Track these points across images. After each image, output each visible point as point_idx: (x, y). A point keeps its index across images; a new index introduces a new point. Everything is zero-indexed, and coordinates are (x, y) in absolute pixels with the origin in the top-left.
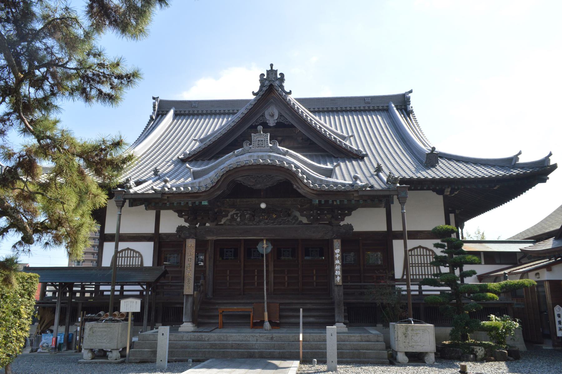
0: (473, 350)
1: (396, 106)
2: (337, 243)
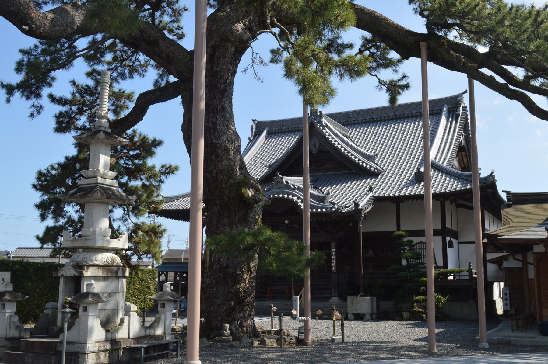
2: (333, 245)
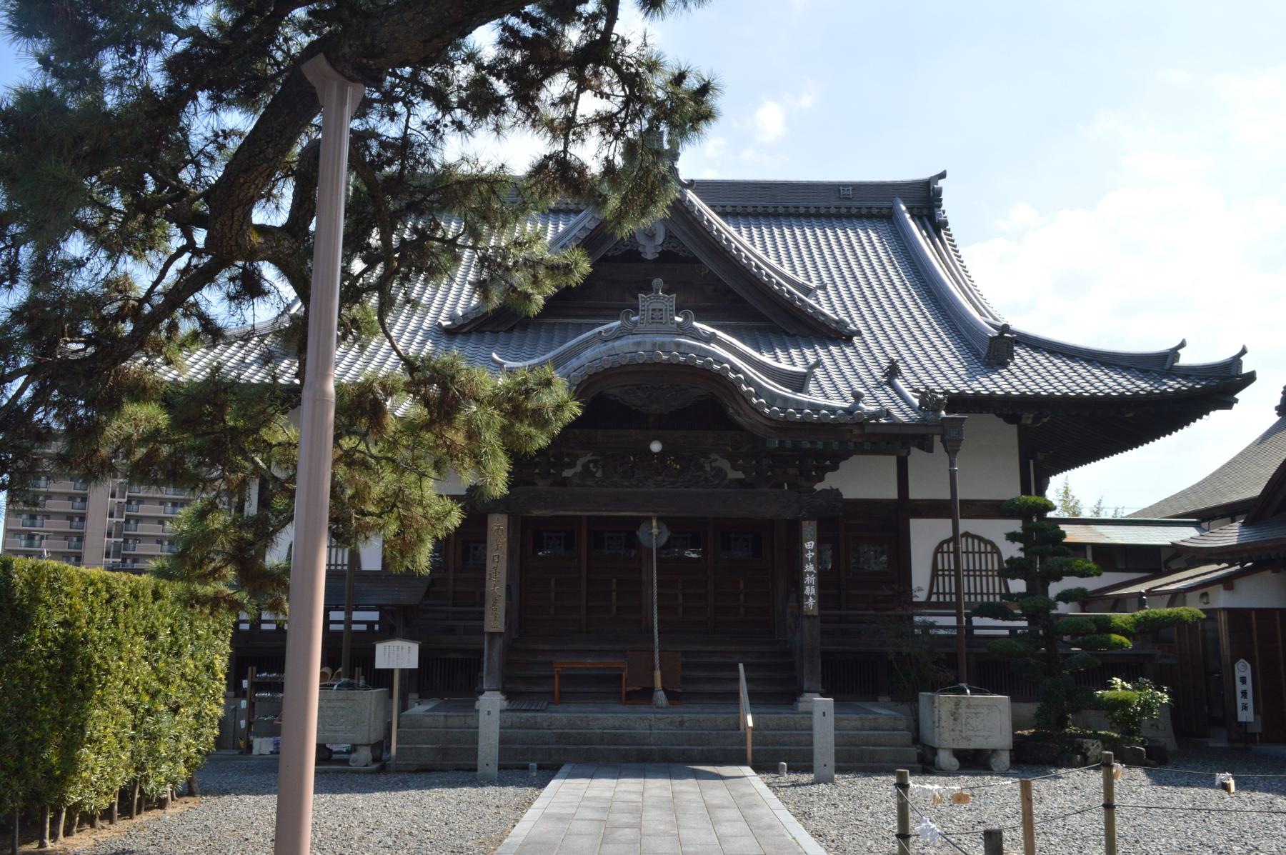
0: (1081, 746)
1: (910, 210)
2: (809, 528)
